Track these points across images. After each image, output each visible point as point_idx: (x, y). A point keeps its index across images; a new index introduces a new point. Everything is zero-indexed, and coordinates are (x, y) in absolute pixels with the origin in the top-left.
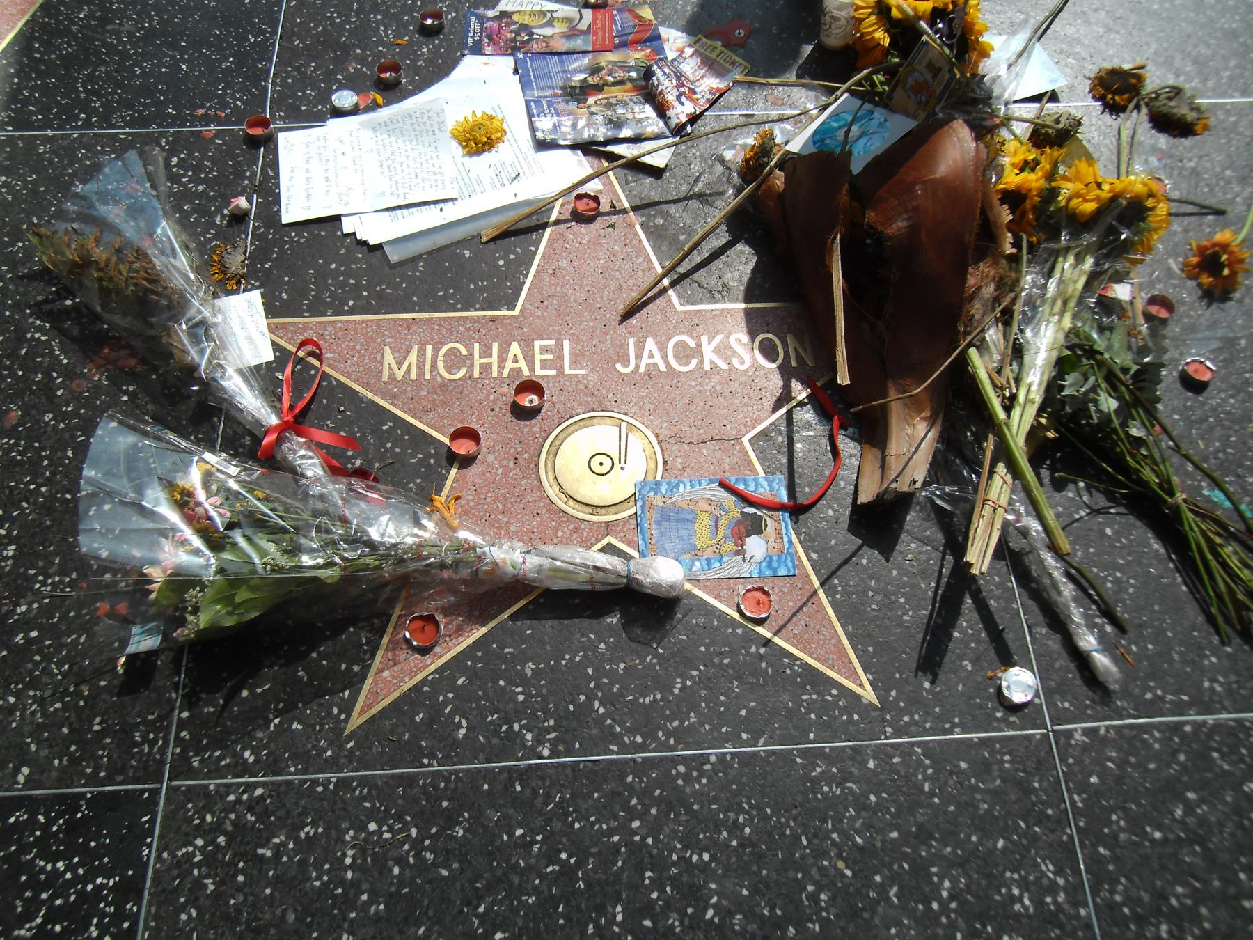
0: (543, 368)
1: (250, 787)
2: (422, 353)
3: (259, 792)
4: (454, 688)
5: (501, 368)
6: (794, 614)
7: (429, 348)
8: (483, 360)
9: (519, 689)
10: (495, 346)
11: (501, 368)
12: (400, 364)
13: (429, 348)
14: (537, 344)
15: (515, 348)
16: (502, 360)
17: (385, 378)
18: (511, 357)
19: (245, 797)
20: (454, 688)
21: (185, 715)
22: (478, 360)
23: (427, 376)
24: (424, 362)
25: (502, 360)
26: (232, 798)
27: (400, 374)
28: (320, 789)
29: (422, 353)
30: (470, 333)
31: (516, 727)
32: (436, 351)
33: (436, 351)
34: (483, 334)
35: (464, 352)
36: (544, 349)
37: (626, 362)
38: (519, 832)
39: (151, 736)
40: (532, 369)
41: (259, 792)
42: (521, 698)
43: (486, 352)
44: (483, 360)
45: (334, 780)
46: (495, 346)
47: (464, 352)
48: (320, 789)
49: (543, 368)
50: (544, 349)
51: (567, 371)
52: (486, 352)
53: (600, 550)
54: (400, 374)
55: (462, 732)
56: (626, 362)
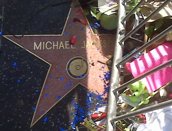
0: (67, 47)
8: (56, 45)
10: (57, 42)
12: (38, 46)
15: (61, 43)
17: (35, 49)
18: (60, 45)
22: (54, 45)
23: (44, 49)
40: (65, 47)
44: (56, 45)
46: (57, 42)
54: (38, 48)
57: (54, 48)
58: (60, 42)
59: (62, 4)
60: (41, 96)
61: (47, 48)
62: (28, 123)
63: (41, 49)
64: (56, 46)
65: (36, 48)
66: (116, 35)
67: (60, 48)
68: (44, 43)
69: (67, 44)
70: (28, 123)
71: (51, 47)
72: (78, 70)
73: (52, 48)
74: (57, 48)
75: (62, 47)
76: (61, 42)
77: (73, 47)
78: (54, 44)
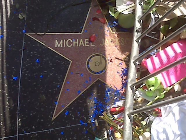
0: (87, 45)
1: (35, 134)
2: (63, 41)
3: (37, 135)
4: (72, 110)
5: (79, 45)
6: (80, 4)
7: (65, 40)
8: (76, 43)
9: (83, 109)
10: (78, 40)
11: (79, 45)
12: (59, 44)
13: (65, 40)
14: (86, 40)
15: (81, 41)
16: (79, 43)
17: (56, 46)
18: (80, 43)
19: (34, 136)
20: (72, 110)
21: (20, 120)
22: (74, 43)
23: (64, 46)
24: (64, 43)
25: (79, 43)
26: (31, 137)
27: (59, 46)
28: (48, 133)
29: (63, 41)
30: (71, 37)
31: (83, 117)
32: (66, 41)
33: (66, 41)
34: (75, 38)
35: (72, 41)
37: (102, 44)
38: (85, 137)
39: (13, 125)
40: (85, 45)
41: (37, 135)
42: (84, 111)
43: (76, 41)
44: (76, 43)
45: (51, 131)
46: (78, 40)
47: (72, 41)
48: (48, 133)
49: (87, 45)
51: (91, 45)
52: (76, 41)
53: (133, 128)
54: (59, 46)
55: (74, 118)
56: (102, 44)
59: (82, 4)
60: (62, 91)
61: (67, 45)
63: (62, 46)
64: (77, 44)
67: (80, 46)
71: (72, 45)
72: (97, 66)
73: (73, 45)
76: (81, 40)
77: (92, 45)
78: (74, 41)
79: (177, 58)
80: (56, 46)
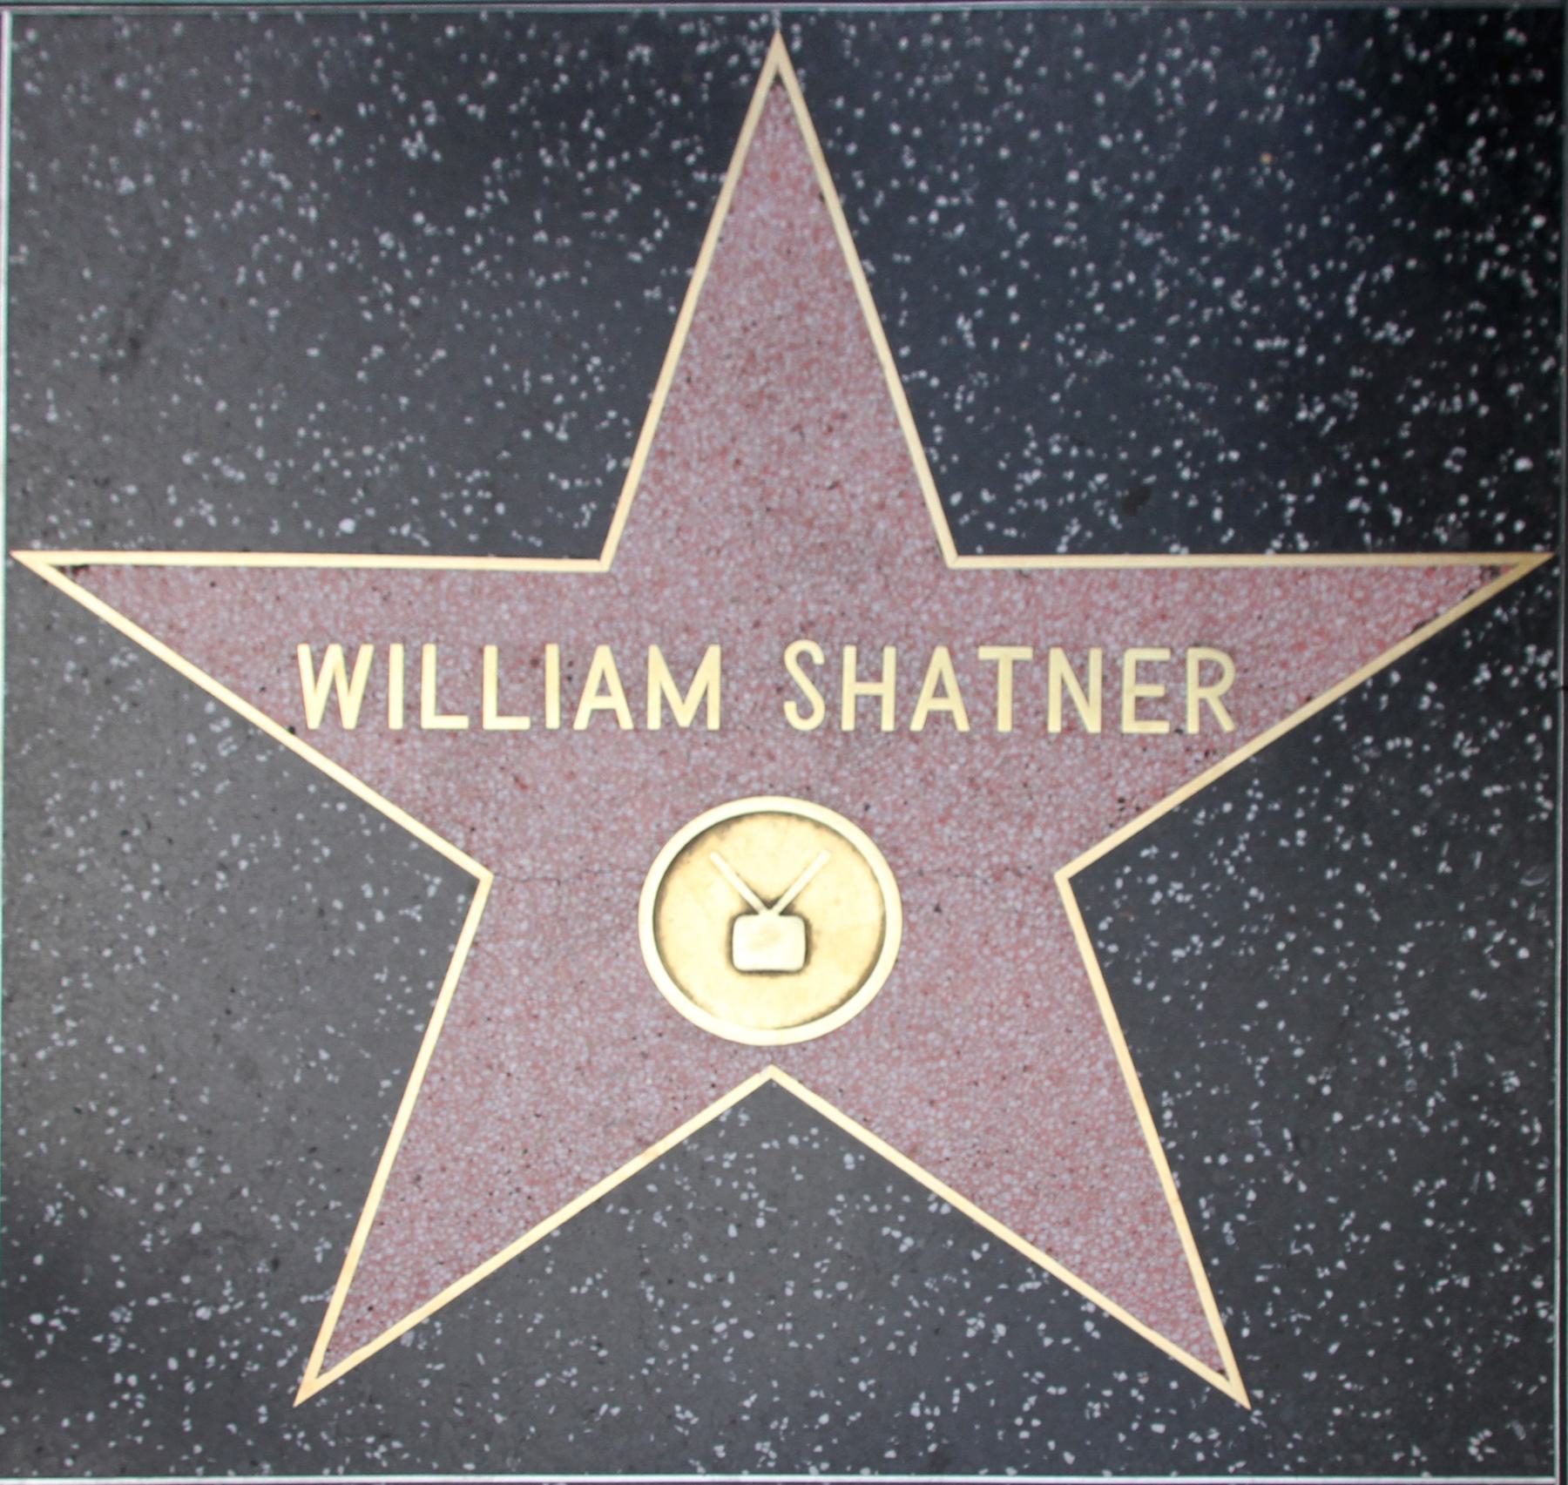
8: (870, 688)
12: (684, 691)
15: (603, 660)
17: (1055, 726)
18: (592, 683)
36: (1147, 672)
44: (870, 688)
50: (1147, 672)
54: (684, 717)
57: (848, 723)
58: (590, 652)
60: (1552, 1096)
62: (1200, 1006)
63: (713, 723)
65: (1081, 672)
66: (1146, 519)
67: (581, 722)
68: (397, 652)
69: (1138, 680)
70: (1200, 1006)
72: (733, 920)
74: (888, 724)
75: (949, 714)
77: (444, 710)
79: (1168, 1327)
80: (1055, 726)
